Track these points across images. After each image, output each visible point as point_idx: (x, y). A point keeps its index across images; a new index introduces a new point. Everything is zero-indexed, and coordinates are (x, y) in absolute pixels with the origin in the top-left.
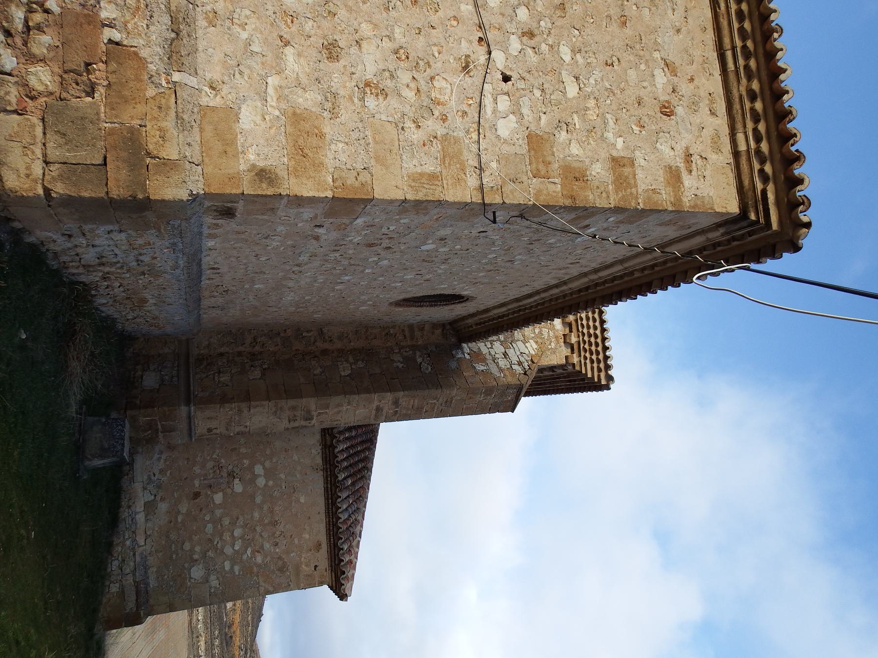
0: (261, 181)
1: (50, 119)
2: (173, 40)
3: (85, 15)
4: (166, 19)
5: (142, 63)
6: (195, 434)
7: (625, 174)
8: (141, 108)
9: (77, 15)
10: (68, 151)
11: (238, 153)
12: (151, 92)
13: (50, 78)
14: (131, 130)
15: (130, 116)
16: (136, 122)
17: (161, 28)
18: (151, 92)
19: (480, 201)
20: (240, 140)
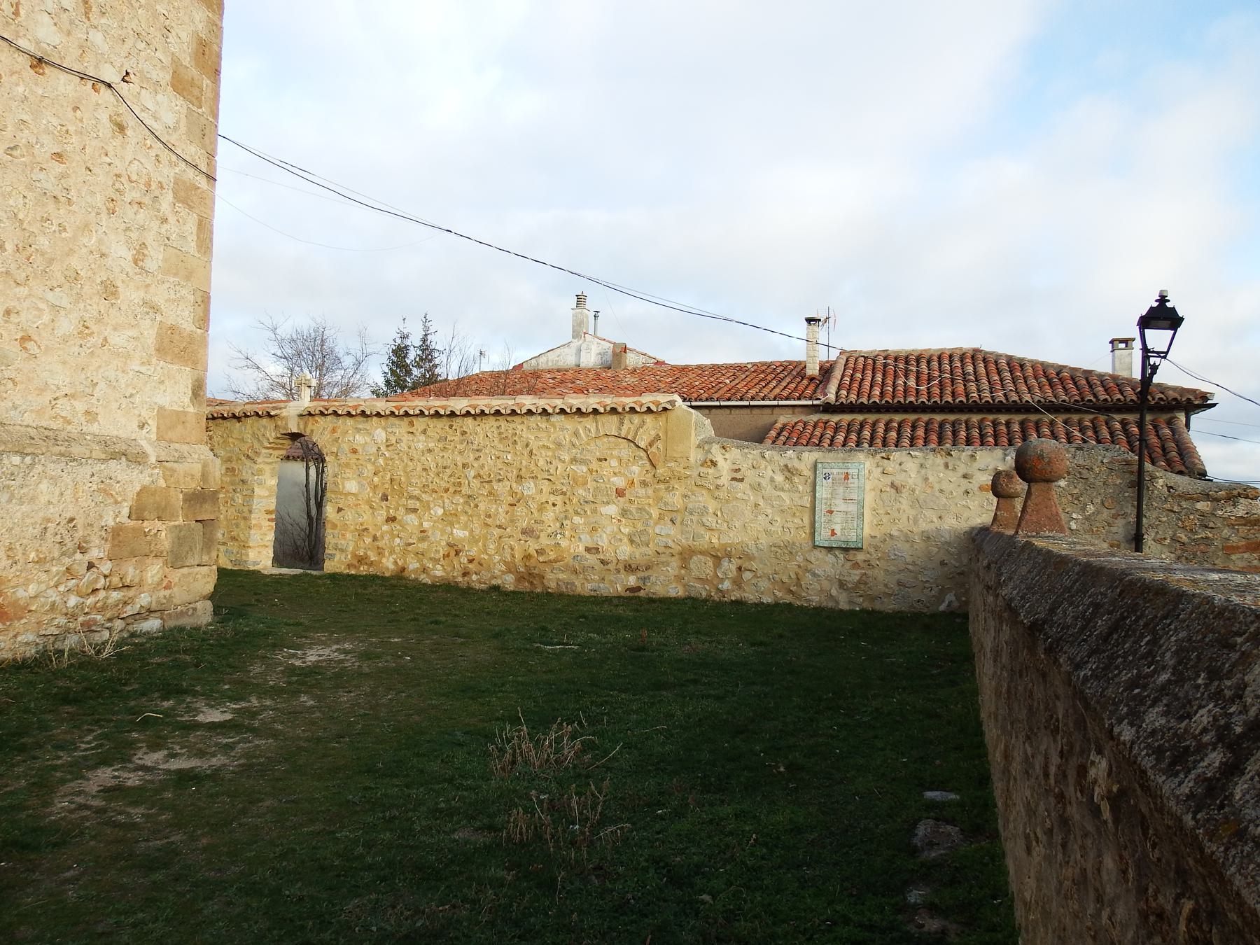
0: (199, 395)
1: (179, 564)
2: (128, 460)
3: (113, 539)
4: (113, 463)
5: (144, 489)
6: (1168, 570)
7: (1118, 481)
8: (172, 493)
9: (114, 546)
10: (196, 548)
11: (184, 412)
12: (162, 483)
13: (155, 566)
14: (185, 500)
15: (178, 499)
16: (181, 496)
17: (117, 469)
18: (162, 483)
19: (1032, 484)
20: (175, 408)
